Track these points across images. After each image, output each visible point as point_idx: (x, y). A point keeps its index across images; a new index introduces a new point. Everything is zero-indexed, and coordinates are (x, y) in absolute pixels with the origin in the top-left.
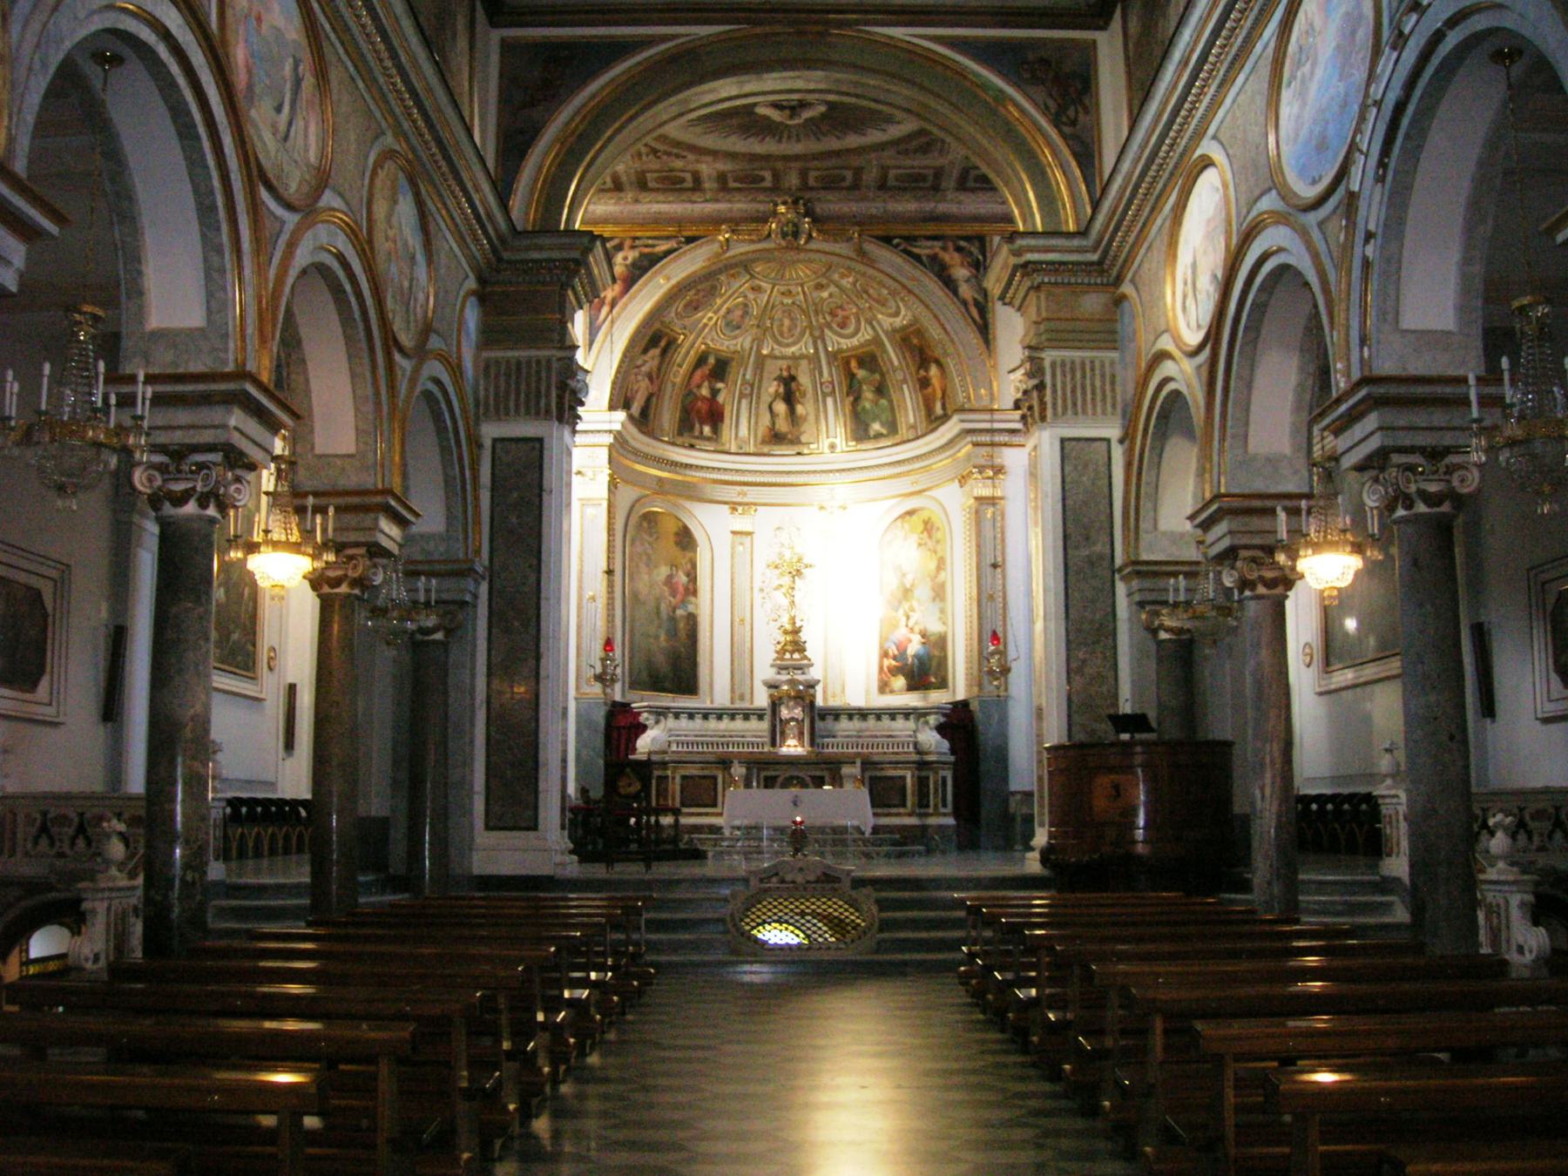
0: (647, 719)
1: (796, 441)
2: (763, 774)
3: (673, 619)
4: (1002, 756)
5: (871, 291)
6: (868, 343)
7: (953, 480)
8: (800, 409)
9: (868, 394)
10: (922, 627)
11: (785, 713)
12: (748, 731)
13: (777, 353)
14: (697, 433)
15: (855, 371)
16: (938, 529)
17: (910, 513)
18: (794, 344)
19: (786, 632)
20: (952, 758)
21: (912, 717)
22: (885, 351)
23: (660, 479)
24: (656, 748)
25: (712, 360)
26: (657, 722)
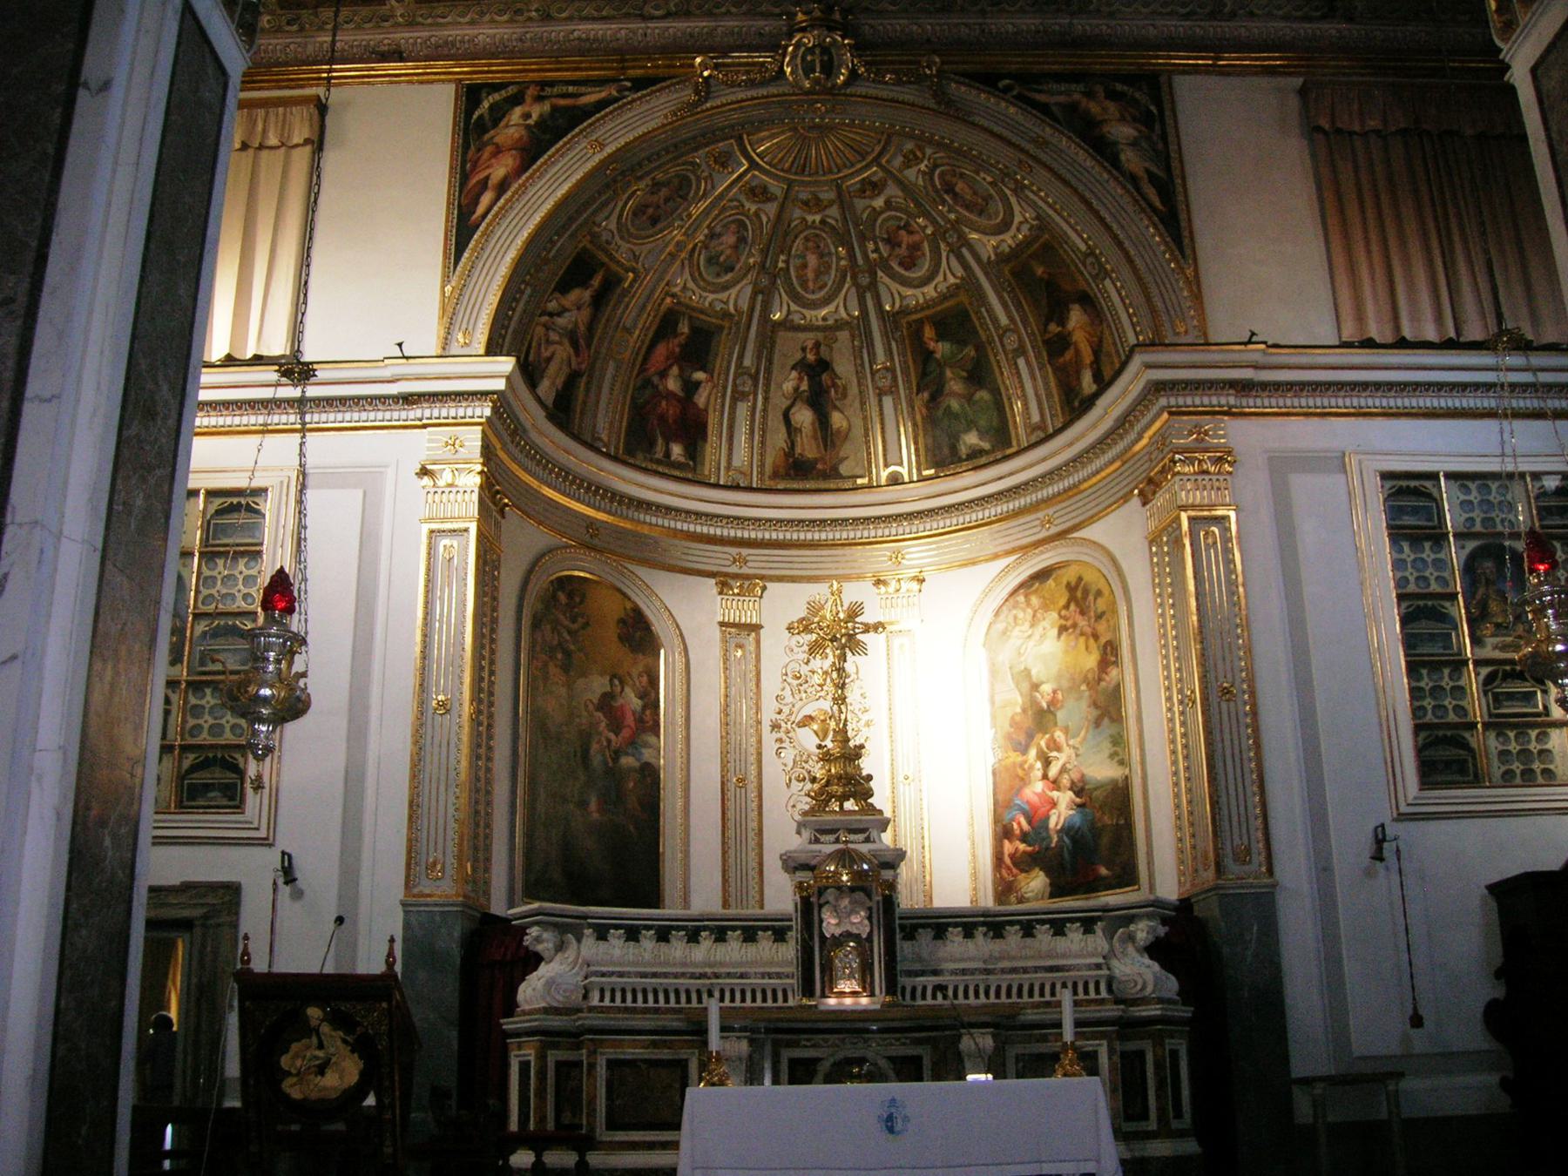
0: (538, 940)
1: (833, 473)
2: (787, 1054)
3: (613, 774)
4: (1271, 1000)
5: (960, 186)
6: (954, 291)
7: (1126, 498)
8: (837, 419)
9: (955, 385)
10: (1075, 776)
11: (831, 924)
12: (754, 963)
13: (796, 319)
14: (659, 455)
15: (932, 345)
16: (1099, 593)
17: (1042, 576)
18: (826, 301)
19: (826, 757)
20: (1186, 1012)
21: (1099, 926)
22: (982, 299)
23: (591, 523)
24: (558, 1000)
25: (684, 328)
26: (560, 947)
